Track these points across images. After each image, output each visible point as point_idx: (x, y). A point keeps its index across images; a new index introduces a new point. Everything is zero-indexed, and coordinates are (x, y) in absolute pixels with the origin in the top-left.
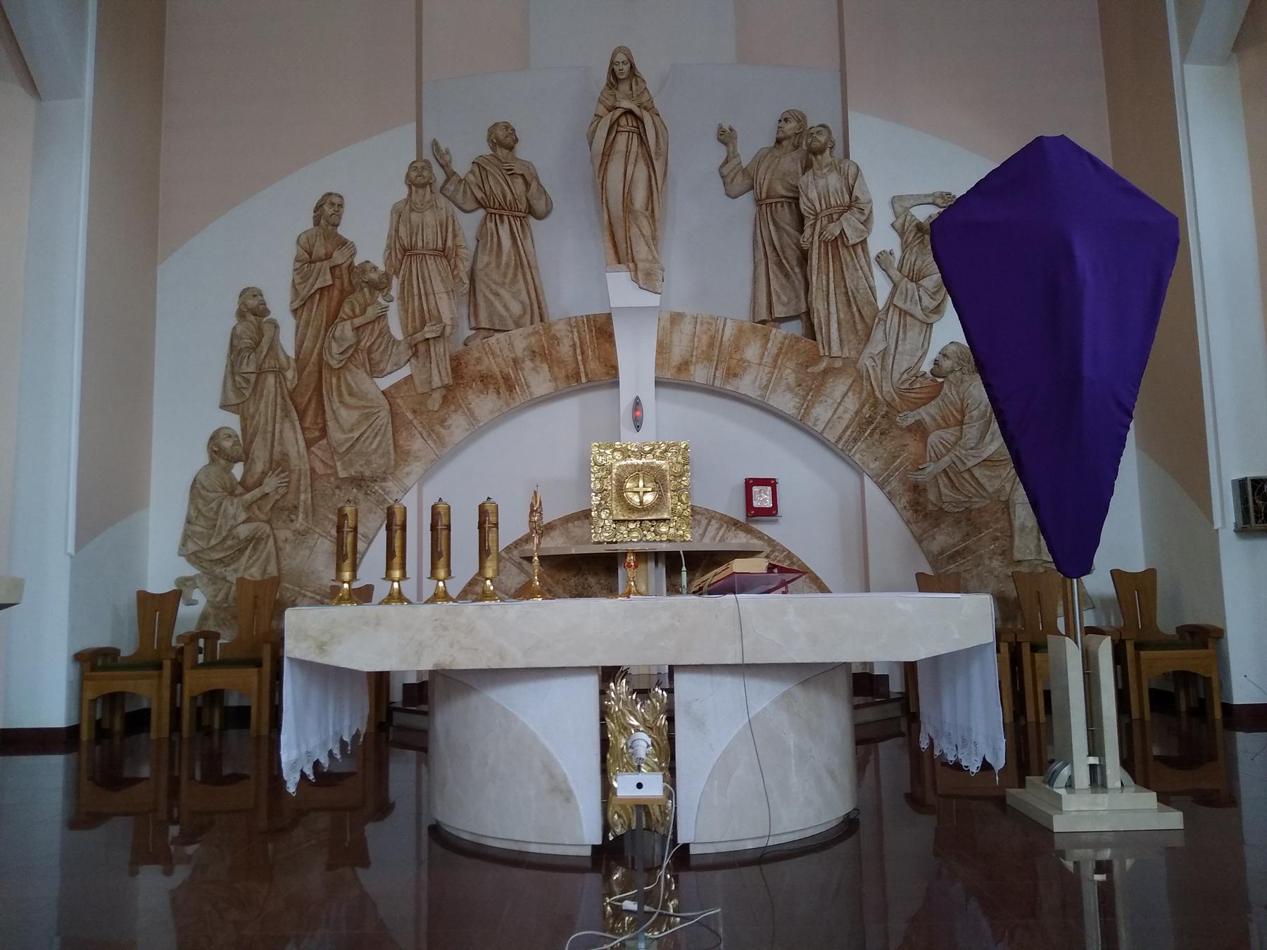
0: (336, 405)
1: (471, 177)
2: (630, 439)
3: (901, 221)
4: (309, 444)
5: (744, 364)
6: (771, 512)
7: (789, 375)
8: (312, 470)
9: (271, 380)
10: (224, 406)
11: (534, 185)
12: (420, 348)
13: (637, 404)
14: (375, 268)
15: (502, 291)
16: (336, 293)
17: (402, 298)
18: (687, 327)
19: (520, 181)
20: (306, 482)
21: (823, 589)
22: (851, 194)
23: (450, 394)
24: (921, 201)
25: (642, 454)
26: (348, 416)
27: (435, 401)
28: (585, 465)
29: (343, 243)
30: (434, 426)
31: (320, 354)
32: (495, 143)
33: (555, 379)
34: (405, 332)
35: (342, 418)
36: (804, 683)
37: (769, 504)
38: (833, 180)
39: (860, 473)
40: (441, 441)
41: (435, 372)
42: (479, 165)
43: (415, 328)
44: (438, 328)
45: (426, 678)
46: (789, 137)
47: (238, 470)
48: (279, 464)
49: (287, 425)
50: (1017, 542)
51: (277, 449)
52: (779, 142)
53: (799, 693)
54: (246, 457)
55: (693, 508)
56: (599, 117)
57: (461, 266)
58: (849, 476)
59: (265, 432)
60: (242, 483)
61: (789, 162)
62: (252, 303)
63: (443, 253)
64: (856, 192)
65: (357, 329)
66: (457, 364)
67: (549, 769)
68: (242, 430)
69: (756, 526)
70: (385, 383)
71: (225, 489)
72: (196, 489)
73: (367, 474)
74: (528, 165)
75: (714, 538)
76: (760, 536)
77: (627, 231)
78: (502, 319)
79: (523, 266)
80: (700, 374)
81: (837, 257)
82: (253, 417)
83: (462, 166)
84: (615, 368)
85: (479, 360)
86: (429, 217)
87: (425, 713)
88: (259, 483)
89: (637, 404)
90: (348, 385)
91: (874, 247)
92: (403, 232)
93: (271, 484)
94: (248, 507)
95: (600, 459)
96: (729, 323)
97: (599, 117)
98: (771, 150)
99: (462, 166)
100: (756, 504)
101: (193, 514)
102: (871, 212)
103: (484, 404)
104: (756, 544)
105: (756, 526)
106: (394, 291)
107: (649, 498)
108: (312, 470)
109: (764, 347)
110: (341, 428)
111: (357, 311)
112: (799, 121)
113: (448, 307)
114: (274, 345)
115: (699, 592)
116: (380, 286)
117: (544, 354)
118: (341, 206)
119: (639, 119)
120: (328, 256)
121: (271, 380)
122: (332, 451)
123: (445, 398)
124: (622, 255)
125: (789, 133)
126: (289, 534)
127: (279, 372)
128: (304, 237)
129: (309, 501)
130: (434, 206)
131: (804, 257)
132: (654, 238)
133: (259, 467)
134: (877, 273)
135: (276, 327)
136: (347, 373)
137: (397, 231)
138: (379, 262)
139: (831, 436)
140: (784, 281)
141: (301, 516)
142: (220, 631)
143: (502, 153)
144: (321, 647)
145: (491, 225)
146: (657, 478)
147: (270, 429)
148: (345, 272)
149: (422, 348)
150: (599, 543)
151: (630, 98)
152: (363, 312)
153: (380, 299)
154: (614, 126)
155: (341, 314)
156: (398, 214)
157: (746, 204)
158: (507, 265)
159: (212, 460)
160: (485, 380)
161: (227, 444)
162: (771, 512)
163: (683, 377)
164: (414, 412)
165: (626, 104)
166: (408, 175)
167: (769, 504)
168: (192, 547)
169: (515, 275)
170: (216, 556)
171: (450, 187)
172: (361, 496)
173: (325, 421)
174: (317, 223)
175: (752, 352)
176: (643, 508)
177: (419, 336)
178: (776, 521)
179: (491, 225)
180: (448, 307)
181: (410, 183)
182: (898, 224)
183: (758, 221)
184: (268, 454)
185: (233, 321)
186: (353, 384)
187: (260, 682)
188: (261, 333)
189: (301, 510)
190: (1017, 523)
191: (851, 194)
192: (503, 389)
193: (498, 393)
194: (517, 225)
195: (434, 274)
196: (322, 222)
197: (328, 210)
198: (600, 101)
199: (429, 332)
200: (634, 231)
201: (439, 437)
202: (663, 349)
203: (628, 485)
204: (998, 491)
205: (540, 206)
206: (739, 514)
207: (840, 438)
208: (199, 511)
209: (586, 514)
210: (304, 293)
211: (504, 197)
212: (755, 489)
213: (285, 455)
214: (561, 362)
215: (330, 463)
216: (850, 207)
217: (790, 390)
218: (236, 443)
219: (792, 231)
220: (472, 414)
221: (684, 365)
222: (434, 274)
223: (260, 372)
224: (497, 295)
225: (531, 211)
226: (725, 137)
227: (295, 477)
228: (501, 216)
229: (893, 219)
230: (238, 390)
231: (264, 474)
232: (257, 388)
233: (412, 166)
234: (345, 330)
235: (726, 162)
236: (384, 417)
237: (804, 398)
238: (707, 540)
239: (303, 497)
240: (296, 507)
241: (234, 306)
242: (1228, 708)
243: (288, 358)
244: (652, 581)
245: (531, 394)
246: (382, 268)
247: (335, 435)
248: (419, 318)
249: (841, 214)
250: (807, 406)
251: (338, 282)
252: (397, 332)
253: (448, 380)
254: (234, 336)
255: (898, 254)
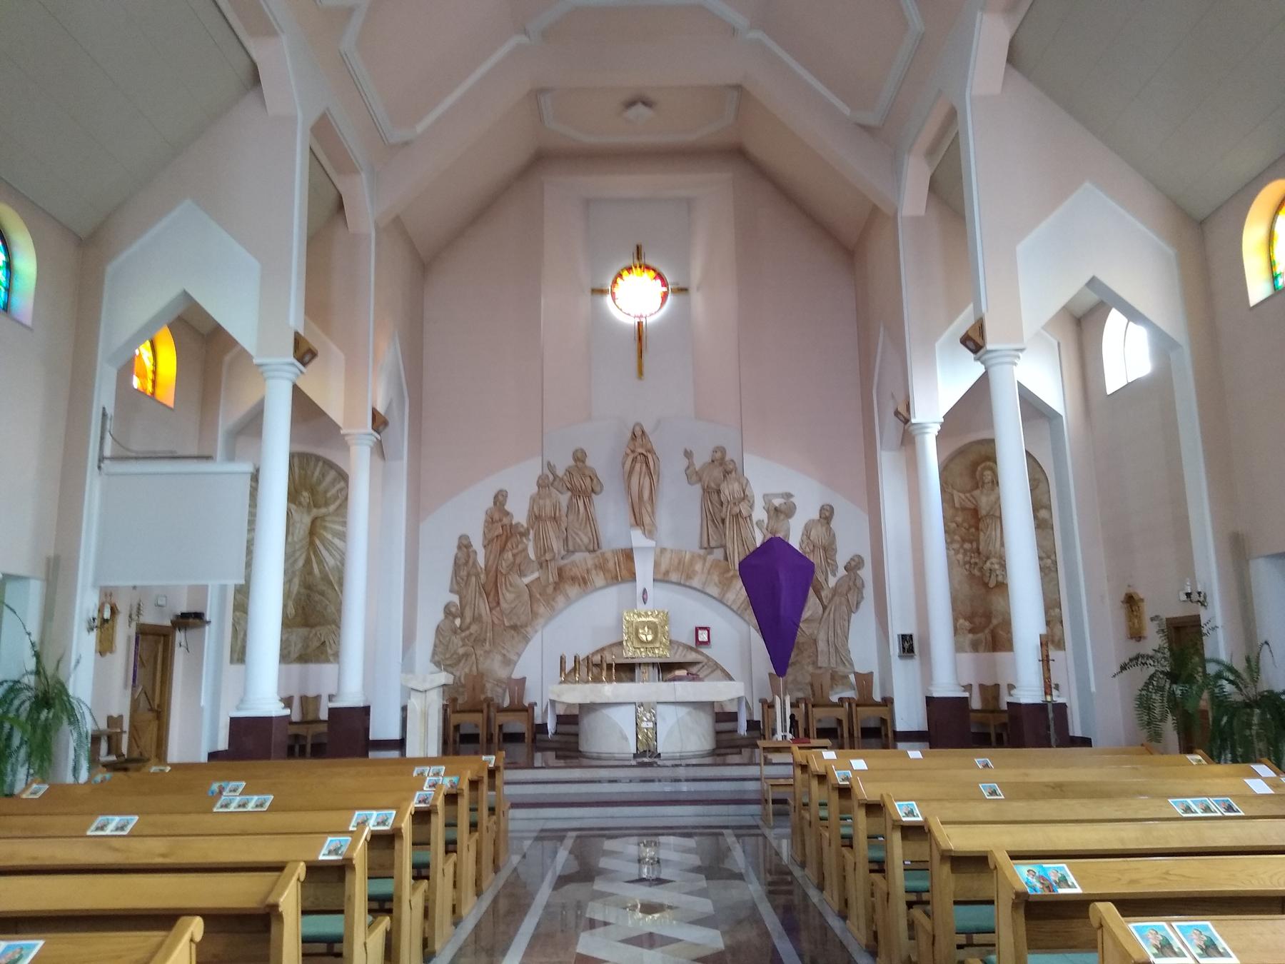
0: (504, 591)
1: (565, 477)
2: (641, 607)
3: (768, 506)
4: (491, 610)
5: (695, 573)
6: (707, 643)
7: (716, 578)
8: (493, 621)
9: (473, 579)
10: (452, 591)
11: (595, 480)
12: (542, 564)
13: (645, 591)
14: (522, 526)
15: (580, 533)
16: (504, 537)
17: (535, 540)
18: (668, 555)
19: (589, 479)
20: (490, 627)
21: (731, 679)
22: (744, 493)
23: (557, 587)
24: (776, 496)
25: (647, 615)
26: (509, 596)
27: (550, 590)
28: (620, 620)
29: (507, 514)
30: (549, 601)
31: (497, 568)
32: (576, 459)
33: (606, 579)
34: (536, 556)
35: (507, 597)
36: (695, 709)
37: (706, 639)
38: (736, 486)
39: (748, 624)
40: (553, 608)
41: (550, 577)
42: (569, 472)
43: (541, 555)
44: (552, 555)
45: (576, 712)
46: (717, 460)
47: (458, 622)
48: (477, 619)
49: (481, 601)
50: (819, 658)
51: (476, 612)
52: (713, 461)
53: (694, 711)
54: (462, 616)
55: (670, 641)
56: (627, 455)
57: (562, 525)
58: (744, 625)
59: (471, 604)
60: (460, 628)
61: (717, 473)
62: (465, 542)
63: (555, 519)
64: (747, 492)
65: (514, 556)
66: (560, 571)
67: (621, 732)
68: (460, 603)
69: (699, 649)
70: (527, 580)
71: (452, 630)
72: (439, 630)
73: (519, 624)
74: (592, 470)
75: (680, 655)
76: (702, 654)
77: (640, 509)
78: (579, 546)
79: (590, 520)
80: (674, 577)
81: (738, 522)
82: (465, 597)
83: (560, 472)
84: (635, 574)
85: (571, 570)
86: (548, 502)
87: (659, 680)
88: (468, 628)
89: (645, 591)
90: (510, 582)
91: (755, 518)
92: (536, 509)
93: (474, 628)
94: (463, 640)
95: (627, 618)
96: (687, 553)
97: (627, 455)
98: (710, 463)
99: (560, 472)
100: (700, 639)
101: (438, 642)
102: (754, 502)
103: (573, 591)
104: (699, 658)
105: (699, 649)
106: (531, 536)
107: (650, 638)
108: (493, 621)
109: (704, 564)
110: (506, 601)
111: (514, 546)
112: (722, 452)
113: (557, 545)
114: (475, 562)
115: (666, 681)
116: (525, 534)
117: (601, 567)
118: (507, 496)
119: (646, 457)
120: (501, 520)
121: (473, 579)
122: (502, 612)
123: (555, 589)
124: (638, 522)
125: (717, 458)
126: (482, 652)
127: (477, 575)
128: (489, 511)
129: (492, 637)
130: (550, 495)
131: (723, 521)
132: (653, 512)
133: (468, 620)
134: (757, 530)
135: (476, 552)
136: (510, 577)
137: (533, 508)
138: (524, 523)
139: (735, 607)
140: (714, 528)
141: (487, 643)
142: (458, 697)
143: (580, 464)
144: (558, 696)
145: (574, 500)
146: (653, 627)
147: (473, 602)
148: (508, 527)
149: (544, 565)
150: (627, 658)
151: (642, 446)
152: (517, 546)
153: (525, 540)
154: (634, 460)
155: (507, 548)
156: (533, 500)
157: (697, 490)
158: (582, 520)
159: (446, 617)
160: (574, 579)
161: (453, 610)
162: (707, 643)
163: (666, 579)
164: (540, 594)
165: (640, 450)
166: (538, 481)
167: (706, 639)
168: (437, 658)
169: (586, 523)
170: (448, 662)
171: (556, 483)
172: (515, 635)
173: (499, 599)
174: (495, 503)
175: (698, 567)
176: (648, 642)
177: (543, 558)
178: (711, 648)
179: (574, 500)
180: (557, 545)
181: (539, 486)
182: (766, 508)
183: (703, 499)
184: (472, 615)
185: (455, 550)
186: (512, 582)
187: (483, 719)
188: (469, 556)
189: (488, 641)
190: (819, 649)
191: (744, 493)
192: (582, 584)
193: (580, 585)
194: (587, 500)
195: (550, 529)
196: (498, 504)
197: (500, 497)
198: (628, 446)
199: (548, 557)
200: (644, 511)
201: (552, 606)
202: (657, 565)
203: (640, 631)
204: (811, 634)
205: (597, 489)
206: (693, 645)
207: (739, 608)
208: (440, 641)
209: (621, 643)
210: (489, 536)
211: (581, 487)
212: (700, 632)
213: (480, 615)
214: (609, 571)
215: (501, 619)
216: (744, 499)
217: (716, 584)
218: (457, 609)
219: (718, 506)
220: (568, 596)
221: (667, 573)
222: (550, 529)
223: (469, 575)
224: (577, 534)
225: (593, 491)
226: (688, 454)
227: (484, 625)
228: (579, 496)
229: (764, 504)
230: (458, 583)
231: (470, 624)
232: (467, 583)
233: (540, 477)
234: (509, 555)
235: (688, 468)
236: (526, 597)
237: (723, 589)
238: (677, 656)
239: (488, 635)
240: (485, 640)
241: (456, 543)
242: (895, 732)
243: (481, 568)
244: (651, 675)
245: (595, 586)
246: (525, 525)
247: (504, 605)
248: (543, 549)
249: (739, 503)
250: (723, 593)
251: (505, 533)
252: (532, 556)
253: (556, 579)
254: (456, 558)
255: (766, 521)
